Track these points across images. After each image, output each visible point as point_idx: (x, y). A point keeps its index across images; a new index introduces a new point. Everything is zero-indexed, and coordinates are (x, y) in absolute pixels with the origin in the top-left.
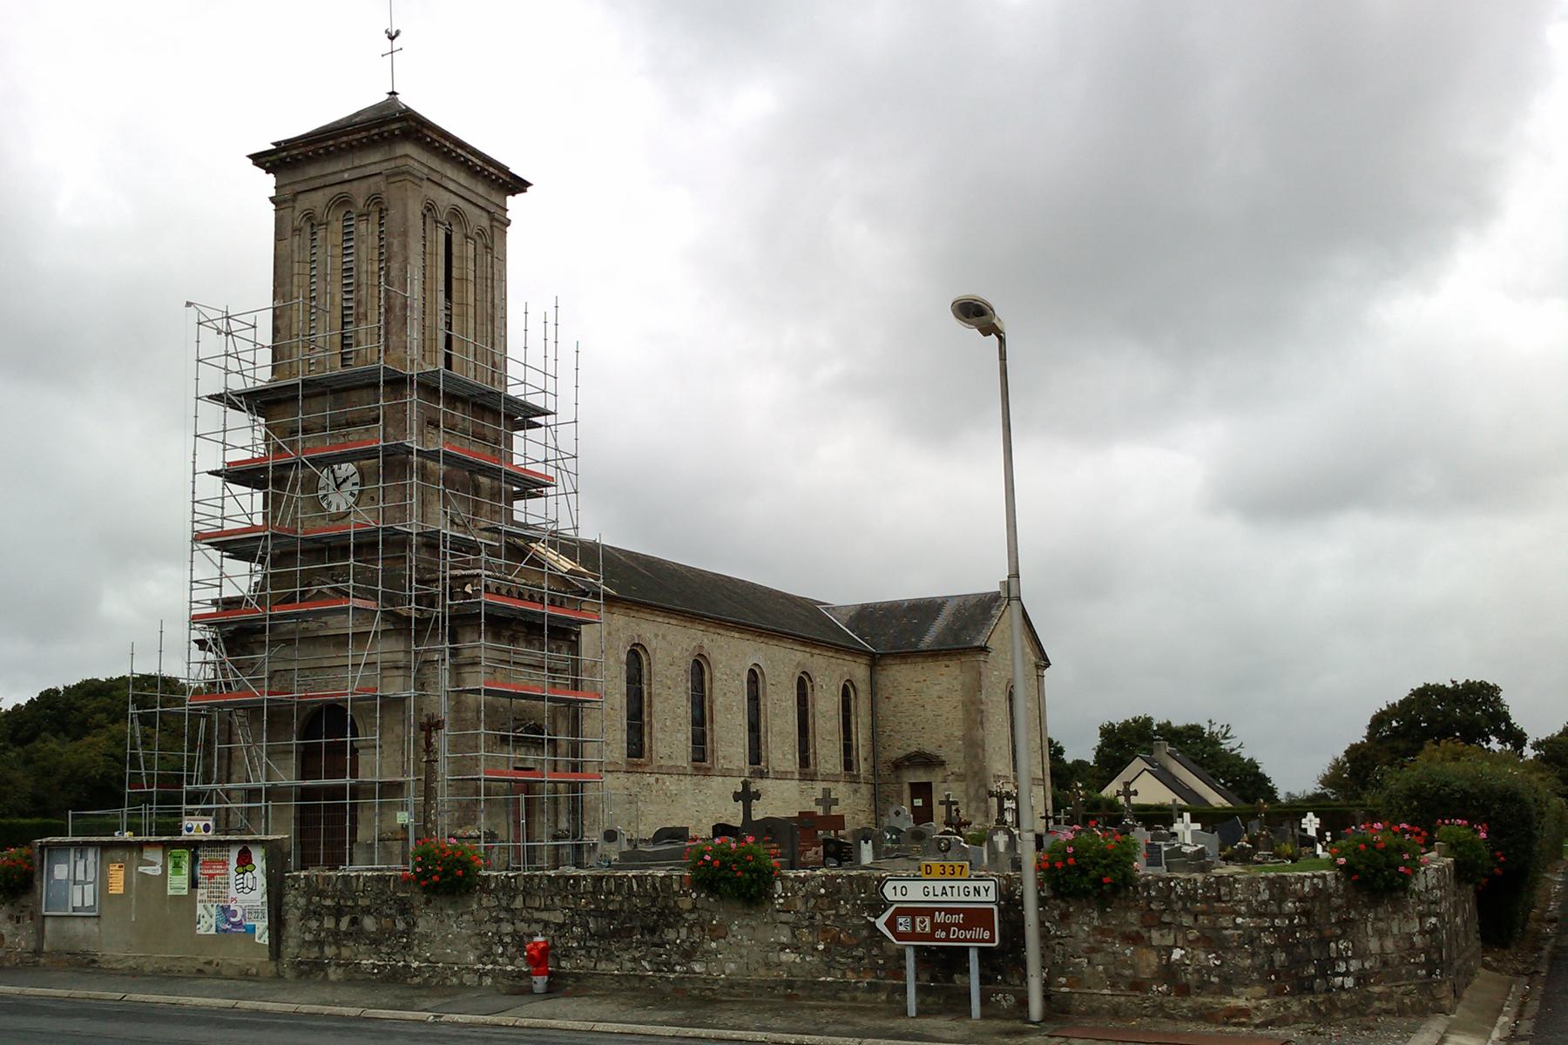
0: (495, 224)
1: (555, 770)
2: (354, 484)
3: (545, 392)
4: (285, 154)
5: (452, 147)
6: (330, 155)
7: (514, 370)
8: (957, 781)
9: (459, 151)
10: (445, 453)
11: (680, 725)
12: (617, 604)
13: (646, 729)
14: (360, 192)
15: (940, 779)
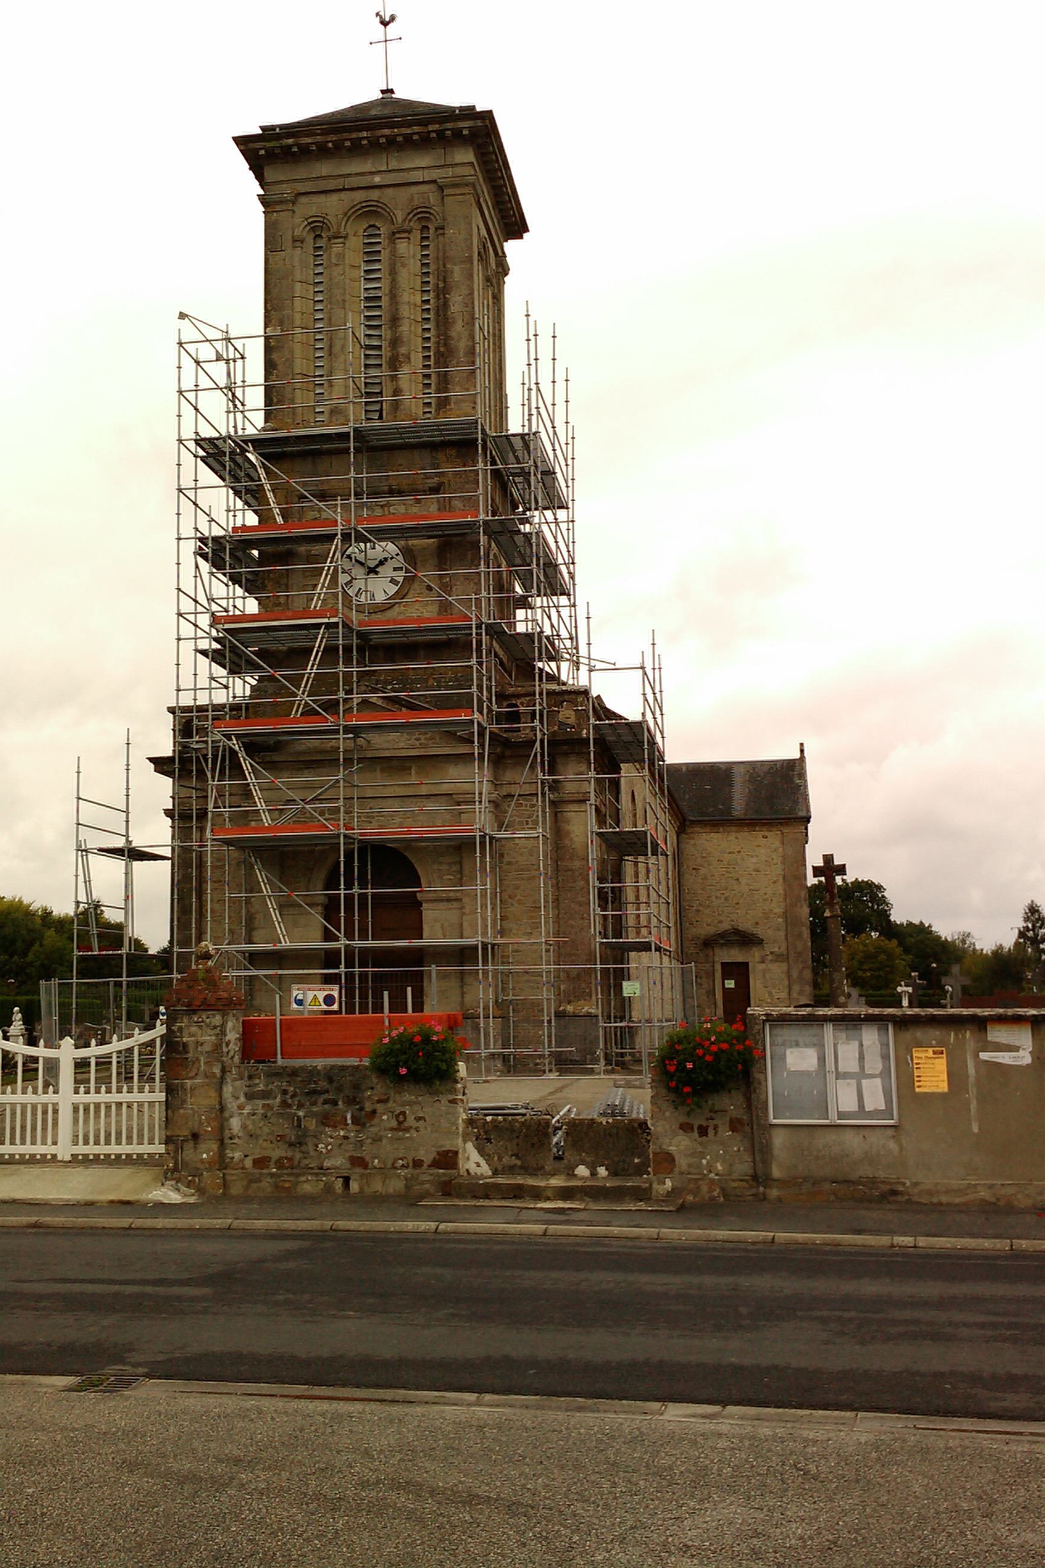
2: (395, 569)
4: (290, 141)
6: (357, 150)
8: (776, 961)
14: (399, 202)
15: (757, 959)
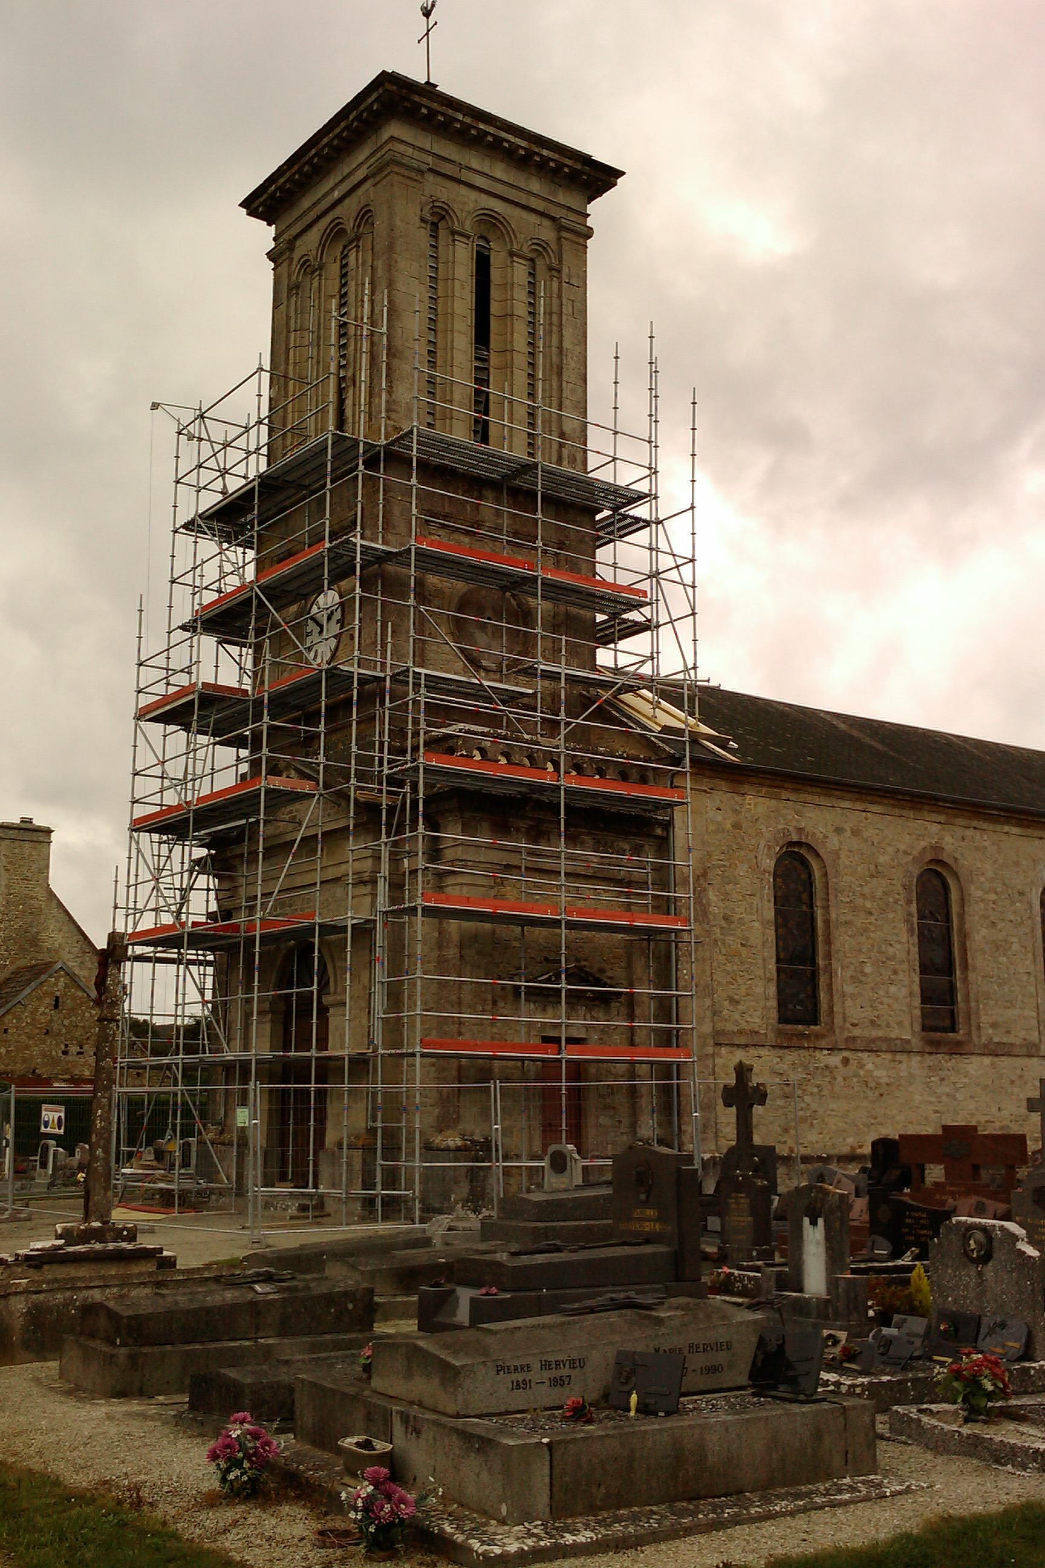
0: (564, 234)
1: (632, 1043)
5: (468, 120)
7: (596, 440)
9: (482, 126)
10: (419, 553)
11: (895, 972)
12: (751, 779)
13: (823, 981)
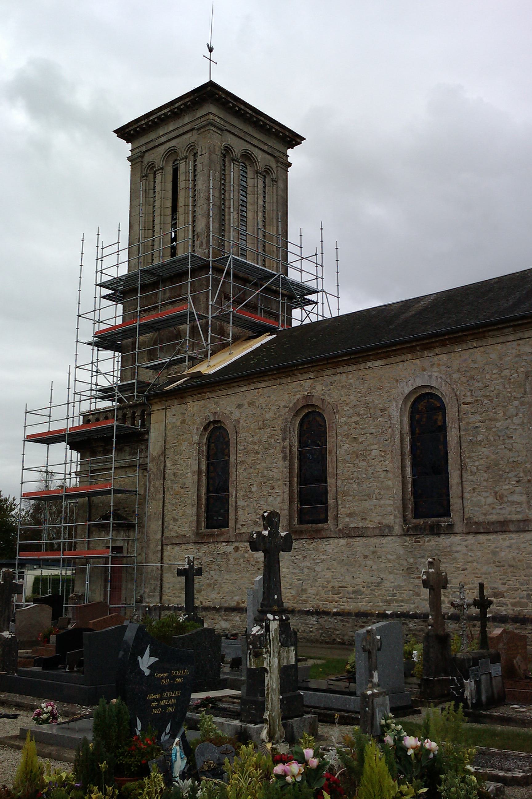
3: (317, 279)
